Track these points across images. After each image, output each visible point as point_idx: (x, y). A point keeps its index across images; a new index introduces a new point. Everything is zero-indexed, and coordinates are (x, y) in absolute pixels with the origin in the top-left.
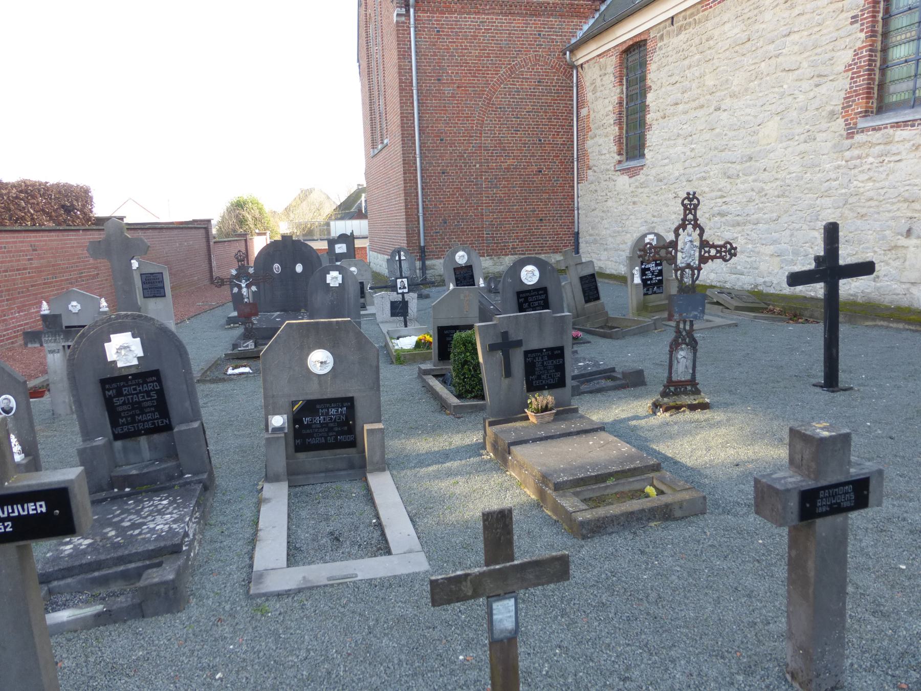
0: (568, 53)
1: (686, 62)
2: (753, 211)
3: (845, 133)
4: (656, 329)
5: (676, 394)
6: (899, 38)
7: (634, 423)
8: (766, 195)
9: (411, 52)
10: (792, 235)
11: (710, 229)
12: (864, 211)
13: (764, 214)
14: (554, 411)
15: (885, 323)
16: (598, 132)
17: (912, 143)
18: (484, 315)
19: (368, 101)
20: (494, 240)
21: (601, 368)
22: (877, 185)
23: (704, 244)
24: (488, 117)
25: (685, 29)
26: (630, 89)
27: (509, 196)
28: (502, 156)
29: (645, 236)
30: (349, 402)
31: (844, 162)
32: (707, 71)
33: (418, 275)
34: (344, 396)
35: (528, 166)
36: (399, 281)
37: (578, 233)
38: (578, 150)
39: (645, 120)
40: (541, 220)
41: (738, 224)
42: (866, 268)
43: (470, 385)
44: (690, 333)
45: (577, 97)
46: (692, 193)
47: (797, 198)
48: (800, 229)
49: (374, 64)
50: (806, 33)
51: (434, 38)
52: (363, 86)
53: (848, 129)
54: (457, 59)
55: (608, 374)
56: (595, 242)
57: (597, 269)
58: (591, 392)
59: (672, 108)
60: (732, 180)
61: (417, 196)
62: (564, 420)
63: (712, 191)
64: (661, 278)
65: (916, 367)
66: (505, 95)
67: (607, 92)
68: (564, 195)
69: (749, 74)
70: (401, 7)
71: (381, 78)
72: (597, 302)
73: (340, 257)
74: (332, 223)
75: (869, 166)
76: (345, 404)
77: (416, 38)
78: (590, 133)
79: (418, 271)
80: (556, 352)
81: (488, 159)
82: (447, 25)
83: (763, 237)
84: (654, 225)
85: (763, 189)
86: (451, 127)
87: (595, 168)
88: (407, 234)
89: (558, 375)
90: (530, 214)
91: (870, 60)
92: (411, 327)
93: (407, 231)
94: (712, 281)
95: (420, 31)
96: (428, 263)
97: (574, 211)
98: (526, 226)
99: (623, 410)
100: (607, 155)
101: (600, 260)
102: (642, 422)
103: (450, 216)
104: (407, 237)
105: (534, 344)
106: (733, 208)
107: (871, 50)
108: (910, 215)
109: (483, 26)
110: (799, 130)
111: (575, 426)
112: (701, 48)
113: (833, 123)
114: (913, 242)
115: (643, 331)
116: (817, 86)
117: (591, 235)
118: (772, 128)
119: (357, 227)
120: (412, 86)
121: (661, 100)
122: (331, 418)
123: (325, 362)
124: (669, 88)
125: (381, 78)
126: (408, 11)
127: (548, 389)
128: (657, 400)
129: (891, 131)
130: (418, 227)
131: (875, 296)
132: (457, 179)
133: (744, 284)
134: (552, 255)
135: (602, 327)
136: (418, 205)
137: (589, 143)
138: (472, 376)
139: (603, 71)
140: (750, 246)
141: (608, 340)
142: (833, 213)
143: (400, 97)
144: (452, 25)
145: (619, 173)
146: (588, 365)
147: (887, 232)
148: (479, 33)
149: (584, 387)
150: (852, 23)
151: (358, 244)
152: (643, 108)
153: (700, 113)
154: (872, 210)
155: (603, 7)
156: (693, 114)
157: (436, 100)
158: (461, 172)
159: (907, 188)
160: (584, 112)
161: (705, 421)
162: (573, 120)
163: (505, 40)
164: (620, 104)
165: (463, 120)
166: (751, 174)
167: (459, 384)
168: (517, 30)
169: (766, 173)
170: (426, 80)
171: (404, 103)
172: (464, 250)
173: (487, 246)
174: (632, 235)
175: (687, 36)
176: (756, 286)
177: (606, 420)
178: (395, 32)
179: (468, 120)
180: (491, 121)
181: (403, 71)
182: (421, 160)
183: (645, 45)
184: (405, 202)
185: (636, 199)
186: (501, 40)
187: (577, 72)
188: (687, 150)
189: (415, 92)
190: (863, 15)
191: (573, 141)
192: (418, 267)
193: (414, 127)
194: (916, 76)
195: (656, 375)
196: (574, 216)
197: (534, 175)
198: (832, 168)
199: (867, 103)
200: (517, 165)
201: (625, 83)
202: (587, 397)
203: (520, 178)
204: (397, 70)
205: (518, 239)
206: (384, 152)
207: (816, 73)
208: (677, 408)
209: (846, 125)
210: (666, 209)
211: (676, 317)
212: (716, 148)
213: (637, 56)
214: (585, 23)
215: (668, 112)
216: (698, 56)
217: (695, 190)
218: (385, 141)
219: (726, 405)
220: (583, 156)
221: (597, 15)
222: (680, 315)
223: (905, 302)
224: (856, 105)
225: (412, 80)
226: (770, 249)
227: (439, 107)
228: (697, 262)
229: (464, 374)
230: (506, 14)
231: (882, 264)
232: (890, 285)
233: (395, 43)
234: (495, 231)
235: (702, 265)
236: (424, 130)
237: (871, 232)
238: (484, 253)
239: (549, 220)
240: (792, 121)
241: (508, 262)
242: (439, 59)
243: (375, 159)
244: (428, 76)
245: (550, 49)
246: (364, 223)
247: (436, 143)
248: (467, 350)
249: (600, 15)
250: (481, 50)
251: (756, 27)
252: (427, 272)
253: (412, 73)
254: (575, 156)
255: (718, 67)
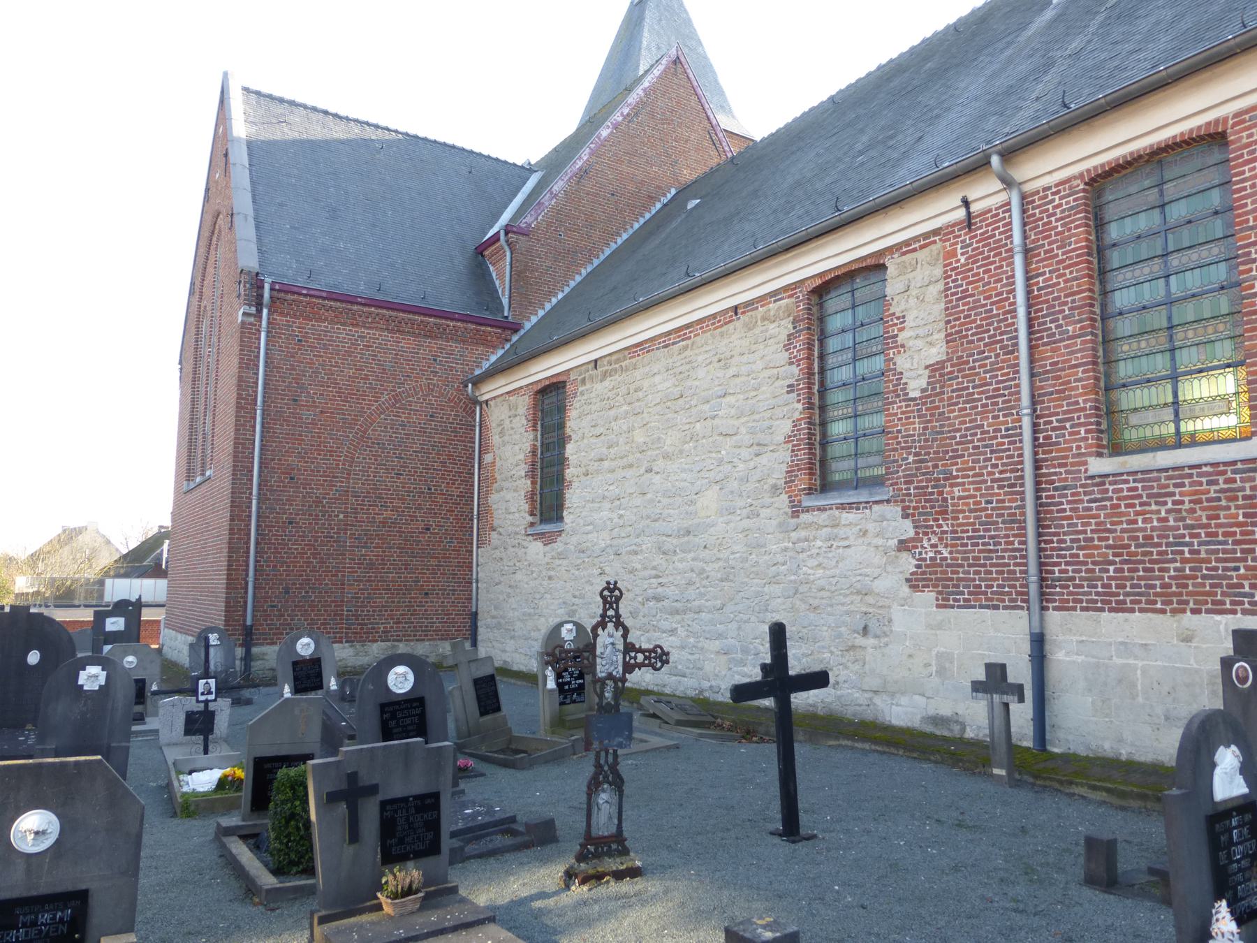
0: (470, 385)
1: (612, 413)
2: (694, 597)
3: (790, 511)
4: (574, 754)
5: (597, 855)
6: (836, 413)
7: (538, 904)
8: (708, 577)
9: (259, 362)
10: (739, 628)
11: (644, 617)
12: (816, 602)
13: (707, 601)
14: (421, 895)
15: (849, 743)
16: (506, 484)
17: (859, 527)
18: (331, 741)
19: (188, 416)
20: (357, 619)
21: (497, 817)
22: (827, 572)
23: (629, 648)
24: (360, 454)
25: (611, 376)
26: (546, 436)
27: (383, 560)
28: (377, 506)
29: (561, 625)
30: (81, 898)
31: (791, 544)
32: (636, 425)
33: (238, 669)
34: (70, 888)
35: (412, 520)
36: (202, 682)
37: (476, 613)
38: (479, 505)
39: (563, 475)
40: (426, 594)
41: (677, 612)
42: (819, 679)
43: (297, 852)
44: (614, 768)
45: (480, 439)
46: (612, 582)
47: (743, 583)
48: (748, 621)
49: (203, 370)
50: (741, 397)
51: (292, 348)
52: (183, 395)
53: (793, 507)
54: (323, 378)
55: (506, 825)
56: (498, 626)
57: (497, 664)
58: (480, 856)
59: (596, 464)
60: (668, 557)
61: (248, 552)
62: (436, 907)
63: (645, 568)
64: (581, 681)
65: (887, 802)
66: (386, 427)
67: (517, 437)
68: (459, 562)
69: (684, 434)
70: (250, 305)
71: (211, 388)
72: (497, 715)
73: (114, 637)
74: (109, 582)
75: (817, 551)
76: (73, 903)
77: (267, 345)
78: (495, 485)
79: (238, 663)
80: (428, 801)
81: (356, 509)
82: (313, 334)
83: (707, 629)
84: (575, 607)
85: (704, 570)
86: (307, 462)
87: (501, 530)
88: (226, 607)
89: (430, 835)
90: (411, 586)
91: (809, 433)
92: (217, 751)
93: (227, 602)
94: (648, 685)
95: (274, 337)
96: (255, 650)
97: (471, 583)
98: (404, 602)
99: (524, 885)
100: (517, 515)
101: (504, 651)
102: (550, 902)
103: (295, 584)
104: (226, 611)
105: (397, 788)
106: (670, 591)
107: (809, 423)
108: (864, 609)
109: (362, 341)
110: (740, 503)
111: (450, 915)
112: (629, 399)
113: (776, 499)
114: (870, 641)
115: (557, 757)
116: (757, 455)
117: (493, 617)
118: (710, 501)
119: (148, 589)
120: (256, 404)
121: (583, 454)
122: (41, 931)
123: (44, 832)
124: (593, 440)
125: (211, 388)
126: (259, 311)
127: (414, 858)
128: (572, 867)
129: (836, 513)
130: (245, 598)
131: (836, 707)
132: (309, 532)
133: (687, 689)
134: (439, 642)
135: (502, 751)
136: (248, 566)
137: (494, 498)
138: (302, 838)
139: (513, 412)
140: (692, 640)
141: (512, 771)
142: (784, 604)
143: (236, 416)
144: (320, 335)
145: (531, 538)
146: (479, 813)
147: (843, 629)
148: (356, 349)
149: (471, 848)
150: (788, 392)
151: (147, 615)
152: (562, 461)
153: (629, 473)
154: (824, 601)
155: (515, 338)
156: (620, 474)
157: (288, 425)
158: (316, 524)
159: (859, 578)
160: (488, 458)
161: (636, 895)
162: (473, 466)
163: (390, 362)
164: (534, 452)
165: (325, 455)
166: (690, 551)
167: (280, 850)
168: (406, 352)
169: (707, 551)
170: (276, 398)
171: (241, 425)
172: (310, 636)
173: (347, 628)
174: (547, 620)
175: (613, 383)
176: (701, 692)
177: (501, 901)
178: (237, 335)
179: (332, 456)
180: (364, 459)
181: (245, 386)
182: (258, 503)
183: (564, 387)
184: (228, 561)
185: (552, 573)
186: (385, 361)
187: (481, 409)
188: (614, 516)
189: (259, 412)
190: (799, 385)
191: (473, 493)
192: (239, 657)
193: (253, 458)
194: (856, 455)
195: (570, 823)
196: (471, 591)
197: (420, 533)
198: (778, 550)
199: (810, 479)
200: (396, 519)
201: (539, 429)
202: (474, 864)
203: (400, 536)
204: (235, 382)
205: (392, 619)
206: (204, 487)
207: (756, 441)
208: (599, 877)
209: (790, 502)
210: (590, 588)
211: (596, 745)
212: (648, 517)
213: (555, 399)
214: (493, 353)
215: (591, 469)
216: (625, 408)
217: (617, 578)
218: (208, 473)
219: (664, 868)
220: (485, 512)
221: (507, 346)
222: (601, 742)
223: (869, 715)
224: (800, 480)
225: (256, 396)
226: (716, 645)
227: (293, 434)
228: (621, 672)
229: (289, 835)
230: (392, 331)
231: (841, 667)
232: (852, 694)
233: (236, 349)
234: (361, 607)
235: (627, 676)
236: (268, 463)
237: (825, 628)
238: (341, 638)
239: (437, 594)
240: (732, 492)
241: (376, 651)
242: (297, 374)
243: (189, 496)
244: (279, 394)
245: (447, 378)
246: (162, 583)
247: (282, 482)
248: (295, 797)
249: (511, 346)
250: (356, 369)
251: (689, 383)
252: (252, 664)
253: (257, 387)
254: (475, 513)
255: (648, 423)
